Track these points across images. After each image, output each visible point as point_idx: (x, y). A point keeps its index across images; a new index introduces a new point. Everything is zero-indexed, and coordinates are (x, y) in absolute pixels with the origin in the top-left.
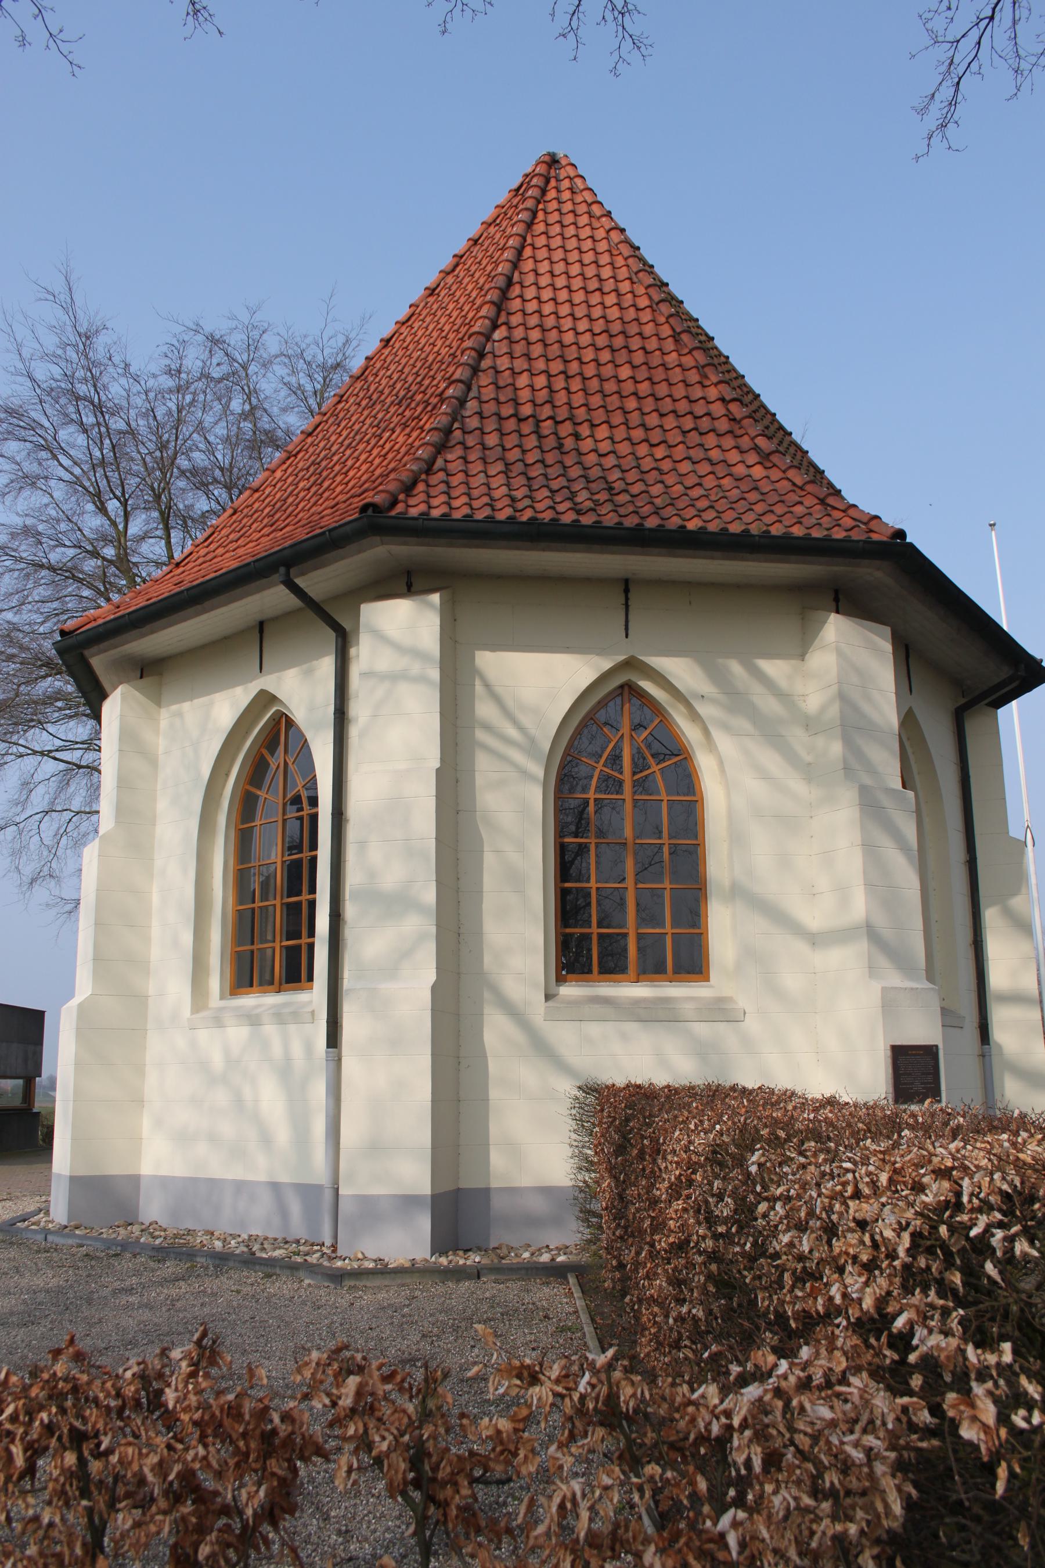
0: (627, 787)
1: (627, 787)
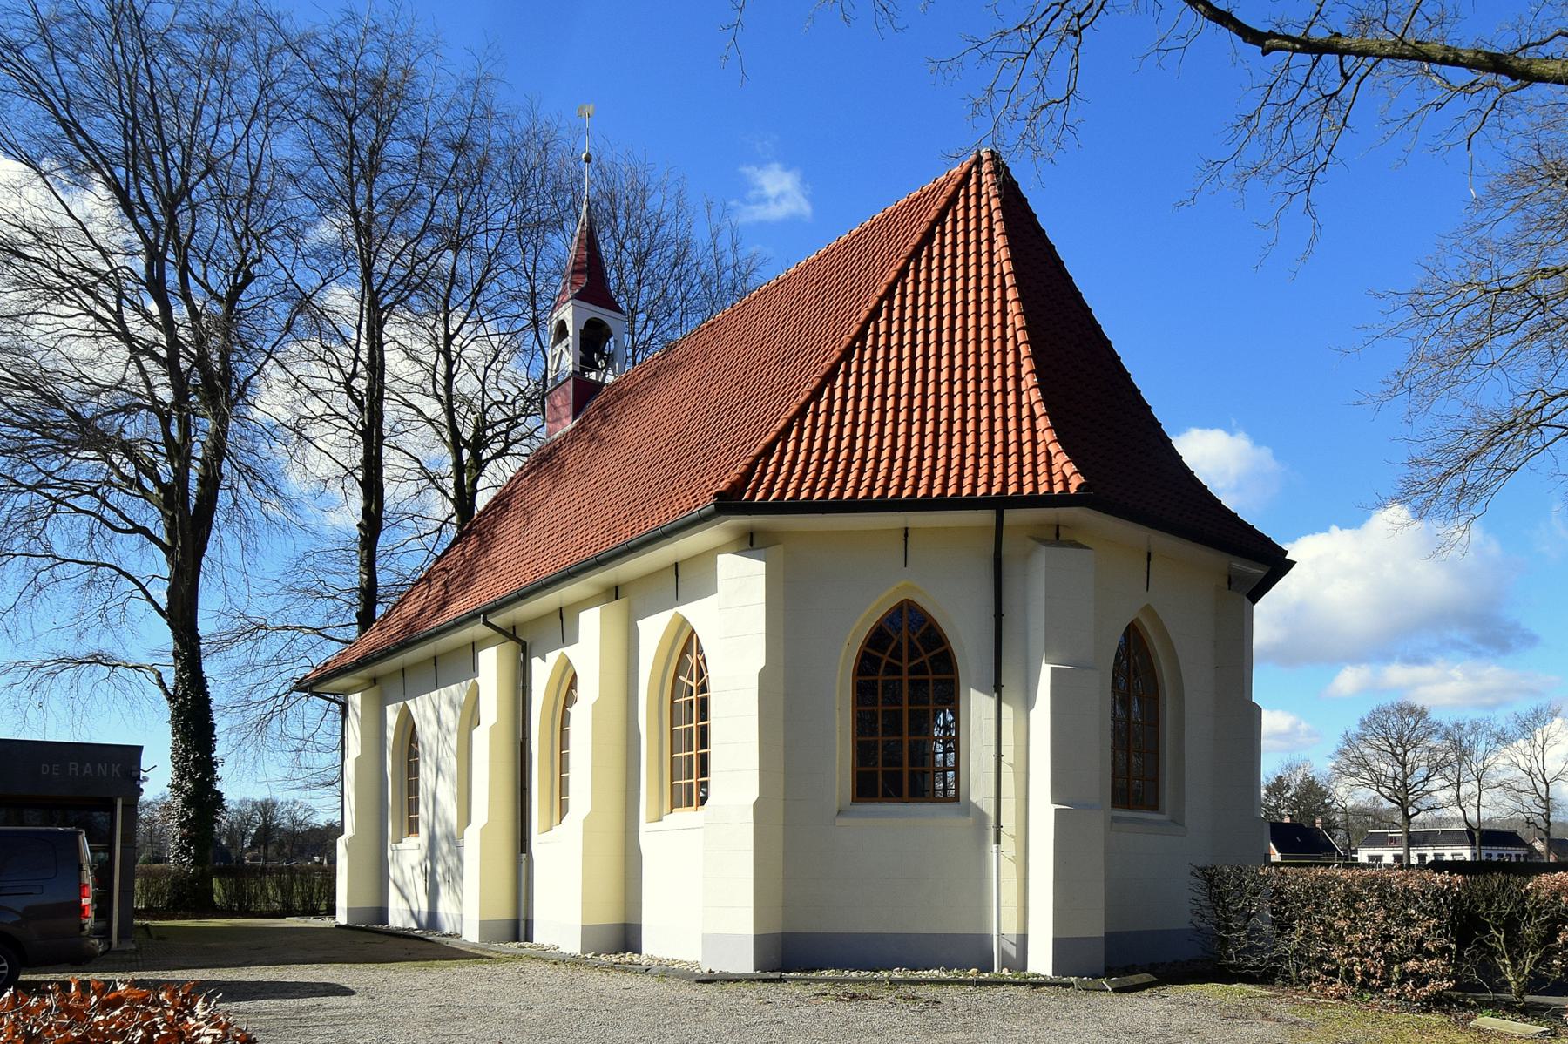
0: (905, 671)
1: (905, 671)
